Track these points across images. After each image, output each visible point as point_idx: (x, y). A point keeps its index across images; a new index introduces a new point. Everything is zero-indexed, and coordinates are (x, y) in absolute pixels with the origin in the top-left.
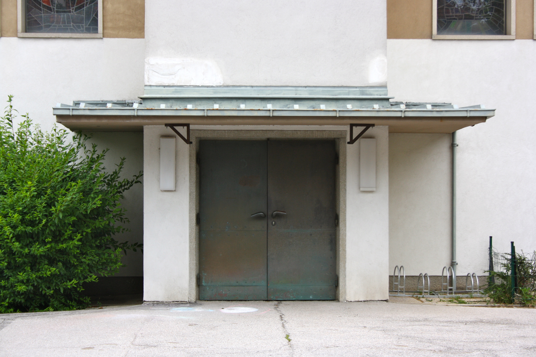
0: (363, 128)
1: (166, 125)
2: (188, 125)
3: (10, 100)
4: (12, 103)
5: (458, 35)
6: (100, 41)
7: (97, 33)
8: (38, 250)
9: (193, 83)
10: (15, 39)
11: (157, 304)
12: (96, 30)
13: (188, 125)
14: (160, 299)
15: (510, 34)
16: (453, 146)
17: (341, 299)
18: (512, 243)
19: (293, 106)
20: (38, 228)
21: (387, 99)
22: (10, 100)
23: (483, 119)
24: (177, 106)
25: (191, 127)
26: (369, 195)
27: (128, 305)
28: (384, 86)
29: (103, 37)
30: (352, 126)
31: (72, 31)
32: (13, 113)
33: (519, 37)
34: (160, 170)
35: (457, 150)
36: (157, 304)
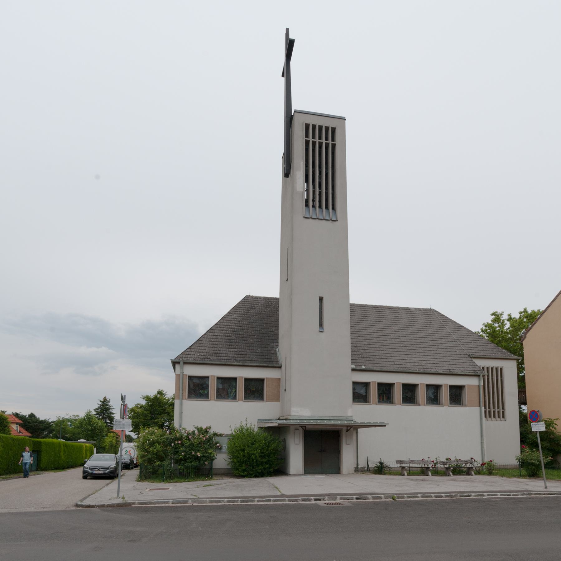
0: (350, 428)
1: (300, 426)
2: (305, 426)
3: (246, 419)
4: (247, 420)
5: (274, 402)
6: (265, 403)
7: (208, 399)
8: (265, 460)
9: (303, 415)
10: (242, 402)
11: (294, 475)
12: (236, 399)
13: (305, 426)
14: (295, 474)
15: (371, 403)
16: (357, 432)
17: (342, 473)
18: (381, 458)
19: (546, 428)
20: (135, 449)
21: (353, 420)
22: (246, 419)
23: (385, 426)
24: (301, 421)
25: (306, 427)
26: (349, 446)
27: (280, 475)
28: (352, 417)
29: (239, 401)
30: (347, 427)
31: (255, 400)
32: (247, 423)
33: (373, 404)
34: (295, 438)
35: (358, 433)
36: (294, 475)
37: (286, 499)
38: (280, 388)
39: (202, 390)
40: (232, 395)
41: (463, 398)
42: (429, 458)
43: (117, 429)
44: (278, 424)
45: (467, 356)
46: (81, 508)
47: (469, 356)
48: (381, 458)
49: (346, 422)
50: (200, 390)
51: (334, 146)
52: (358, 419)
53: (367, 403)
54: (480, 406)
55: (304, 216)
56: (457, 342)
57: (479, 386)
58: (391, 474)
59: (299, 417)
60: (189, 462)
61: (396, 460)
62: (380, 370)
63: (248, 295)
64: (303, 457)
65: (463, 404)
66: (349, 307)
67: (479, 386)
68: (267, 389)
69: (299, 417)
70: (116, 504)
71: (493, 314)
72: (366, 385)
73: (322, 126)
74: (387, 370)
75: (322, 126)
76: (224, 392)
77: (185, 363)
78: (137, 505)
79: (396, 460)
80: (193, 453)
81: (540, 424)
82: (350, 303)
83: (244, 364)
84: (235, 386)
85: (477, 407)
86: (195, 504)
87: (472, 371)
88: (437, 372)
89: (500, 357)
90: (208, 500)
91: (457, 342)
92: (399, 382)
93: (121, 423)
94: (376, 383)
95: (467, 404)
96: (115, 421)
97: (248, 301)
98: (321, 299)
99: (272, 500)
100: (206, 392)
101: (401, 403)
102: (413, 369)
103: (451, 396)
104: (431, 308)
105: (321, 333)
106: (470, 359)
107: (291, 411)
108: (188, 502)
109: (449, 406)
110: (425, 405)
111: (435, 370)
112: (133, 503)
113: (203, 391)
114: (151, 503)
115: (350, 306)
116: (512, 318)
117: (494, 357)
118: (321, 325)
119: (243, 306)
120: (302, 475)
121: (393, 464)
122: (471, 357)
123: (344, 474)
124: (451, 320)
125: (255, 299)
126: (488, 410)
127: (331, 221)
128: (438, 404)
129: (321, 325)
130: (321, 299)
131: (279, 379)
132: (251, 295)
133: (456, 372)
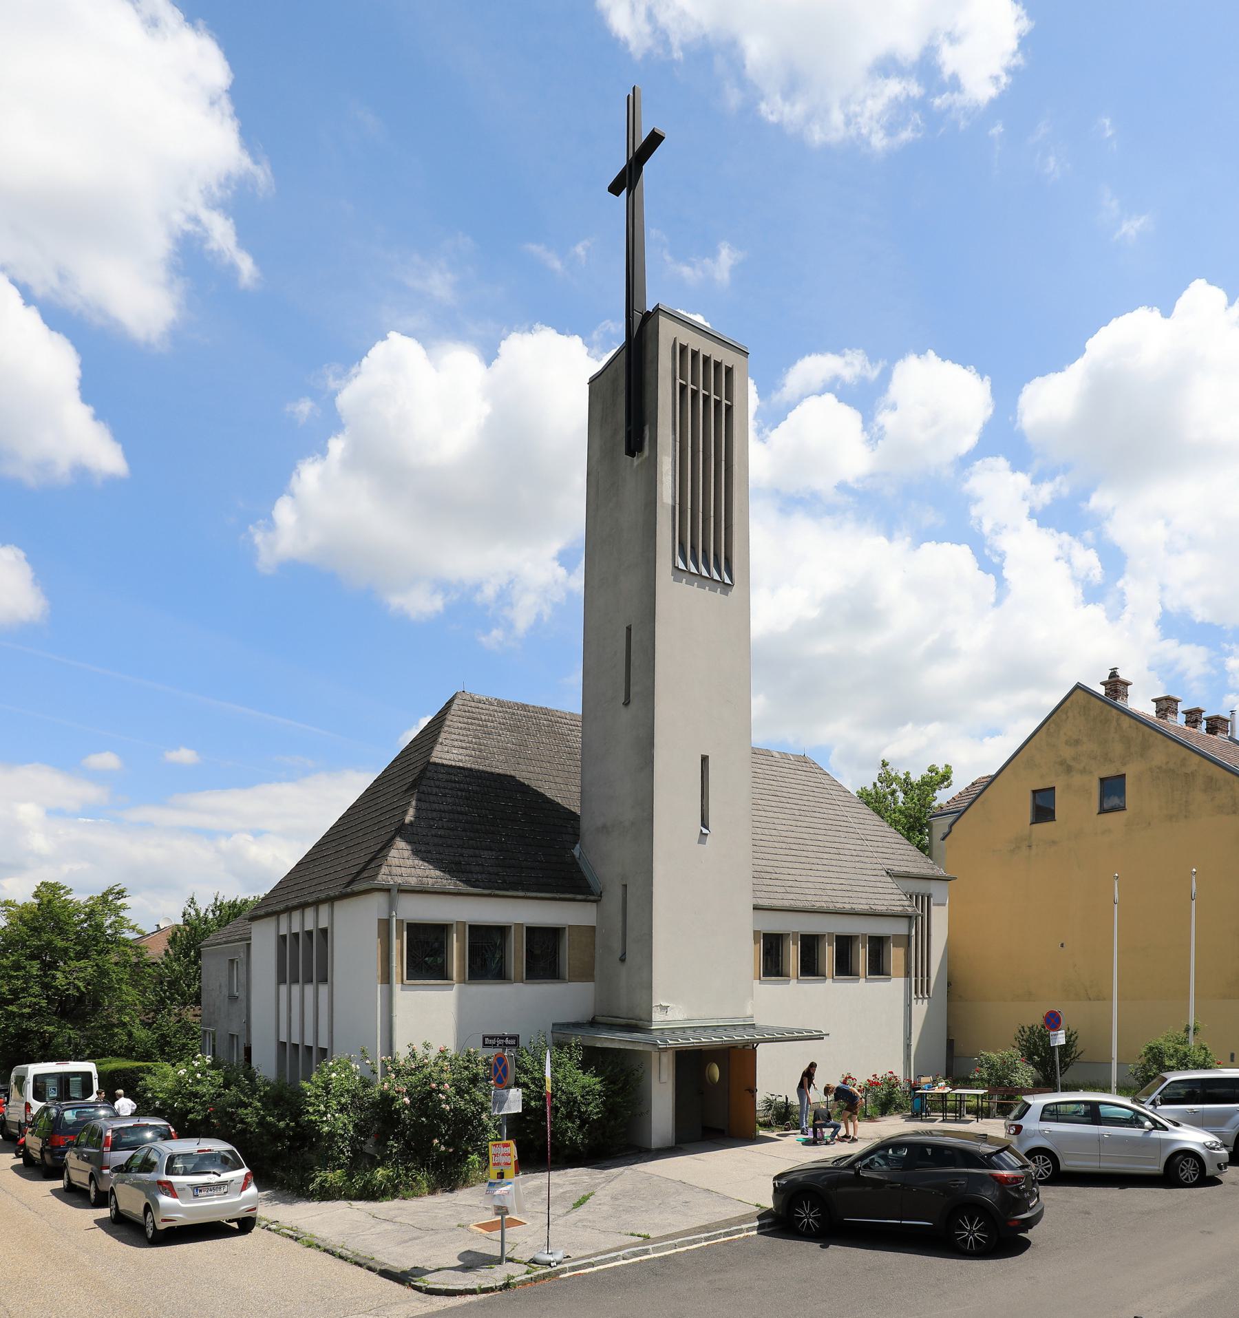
38: (594, 949)
39: (431, 956)
40: (494, 966)
45: (885, 874)
47: (888, 873)
50: (425, 957)
51: (729, 409)
56: (862, 839)
57: (909, 937)
68: (567, 954)
73: (686, 347)
75: (686, 347)
76: (478, 960)
81: (454, 760)
84: (500, 944)
91: (862, 839)
97: (466, 709)
98: (705, 759)
100: (439, 960)
113: (432, 958)
118: (704, 823)
119: (462, 725)
129: (704, 823)
130: (705, 759)
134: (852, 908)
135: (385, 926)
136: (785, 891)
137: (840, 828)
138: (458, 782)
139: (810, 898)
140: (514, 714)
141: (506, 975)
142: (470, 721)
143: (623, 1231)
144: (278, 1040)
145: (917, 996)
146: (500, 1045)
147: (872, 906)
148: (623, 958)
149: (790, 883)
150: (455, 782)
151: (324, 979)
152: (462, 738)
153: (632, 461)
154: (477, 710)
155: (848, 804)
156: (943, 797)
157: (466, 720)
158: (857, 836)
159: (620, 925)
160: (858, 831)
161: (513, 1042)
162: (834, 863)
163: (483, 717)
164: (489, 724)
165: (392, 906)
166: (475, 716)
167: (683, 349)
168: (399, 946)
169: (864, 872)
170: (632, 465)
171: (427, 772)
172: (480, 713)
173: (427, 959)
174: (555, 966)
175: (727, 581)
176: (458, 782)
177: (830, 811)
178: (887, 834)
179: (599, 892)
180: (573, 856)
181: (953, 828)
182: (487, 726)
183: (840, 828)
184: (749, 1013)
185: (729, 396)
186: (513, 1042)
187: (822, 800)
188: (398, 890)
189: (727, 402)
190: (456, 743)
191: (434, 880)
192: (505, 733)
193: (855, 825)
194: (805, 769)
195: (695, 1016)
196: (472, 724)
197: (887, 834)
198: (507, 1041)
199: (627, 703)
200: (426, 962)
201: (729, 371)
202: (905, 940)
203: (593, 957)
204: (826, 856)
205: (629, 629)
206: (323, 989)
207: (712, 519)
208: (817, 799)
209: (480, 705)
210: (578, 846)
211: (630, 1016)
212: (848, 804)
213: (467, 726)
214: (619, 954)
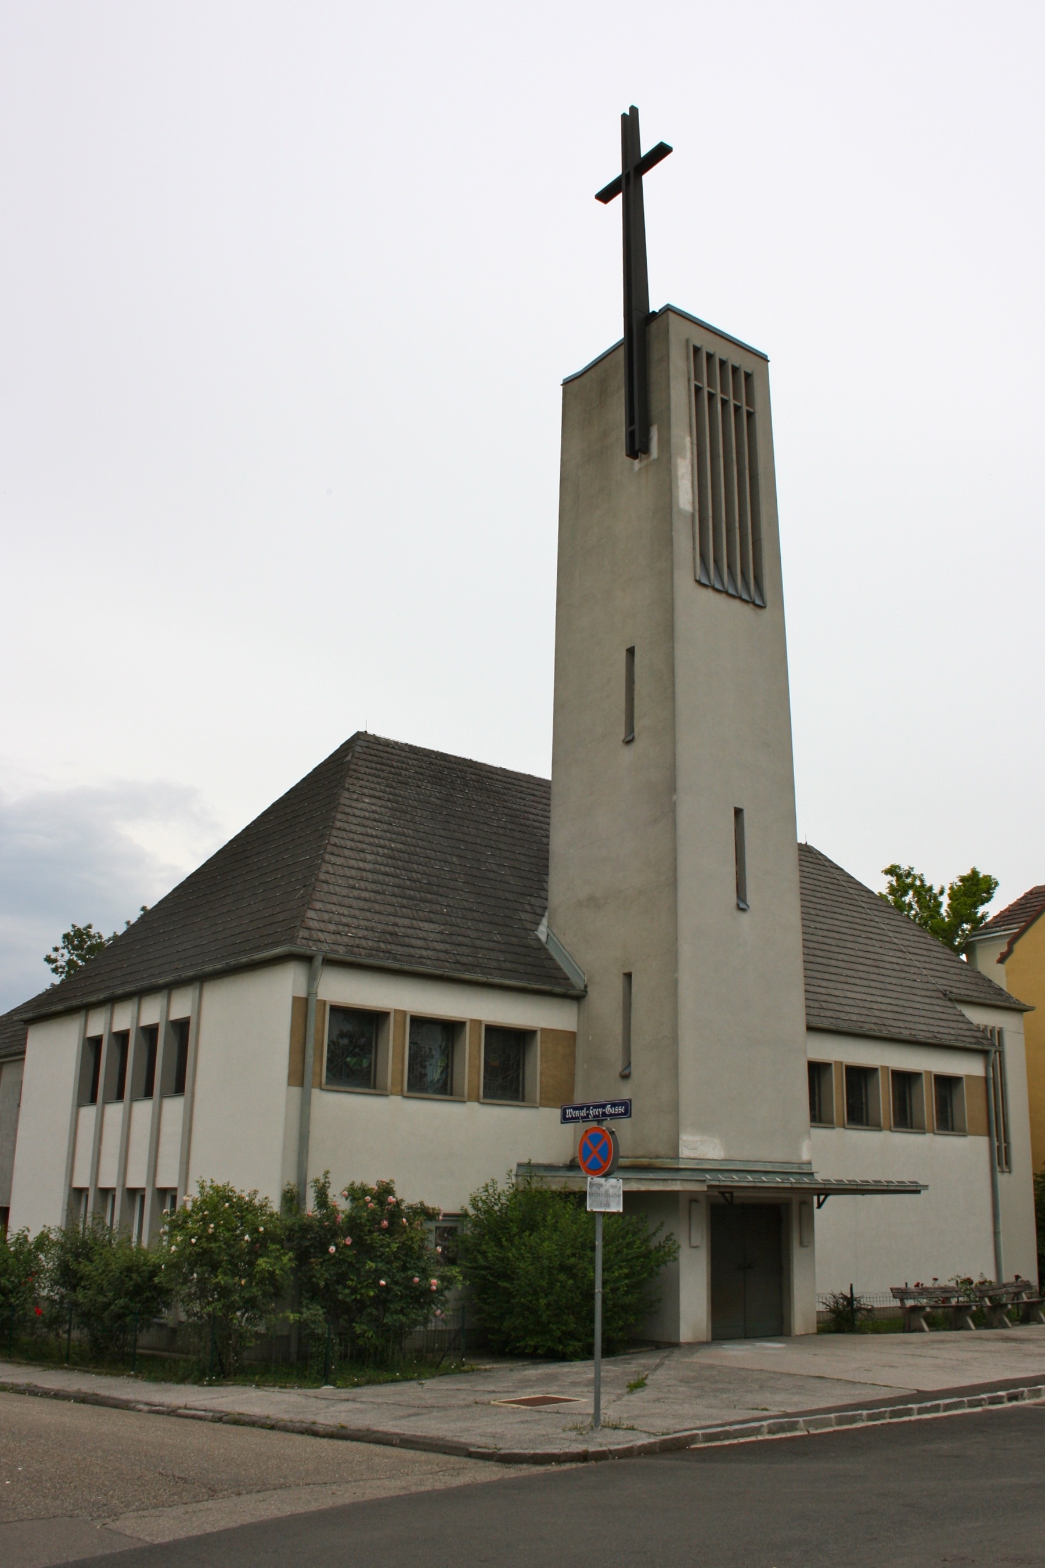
18: (851, 1285)
33: (838, 1126)
37: (963, 1401)
38: (574, 1063)
39: (354, 1055)
41: (955, 1112)
42: (936, 1279)
43: (595, 1210)
44: (709, 1187)
46: (567, 1466)
47: (945, 995)
48: (851, 1285)
49: (750, 1178)
50: (347, 1057)
51: (750, 415)
52: (825, 1173)
53: (516, 1099)
54: (989, 1134)
55: (698, 578)
58: (876, 1331)
59: (698, 1164)
60: (396, 1312)
61: (891, 1289)
62: (832, 1027)
63: (362, 730)
64: (708, 1283)
65: (955, 1128)
66: (797, 853)
67: (986, 1079)
69: (698, 1164)
70: (658, 1445)
71: (892, 871)
72: (451, 1028)
74: (820, 1025)
77: (331, 962)
78: (701, 1442)
79: (891, 1289)
80: (417, 1279)
82: (799, 841)
83: (491, 980)
85: (297, 1086)
86: (813, 1431)
87: (973, 1040)
88: (912, 1038)
89: (993, 1002)
90: (832, 1416)
92: (840, 1060)
93: (603, 1190)
94: (480, 1027)
95: (967, 1128)
96: (591, 1183)
98: (738, 812)
99: (942, 1406)
101: (844, 1121)
102: (867, 1026)
103: (332, 1047)
104: (809, 844)
105: (742, 915)
106: (949, 1004)
107: (681, 1142)
108: (798, 1427)
109: (893, 1129)
110: (934, 1130)
111: (908, 1033)
112: (693, 1438)
113: (355, 1060)
114: (727, 1435)
115: (799, 850)
116: (893, 880)
117: (989, 1002)
119: (373, 771)
120: (707, 1343)
121: (878, 1299)
122: (950, 1000)
123: (797, 1336)
124: (860, 884)
125: (393, 751)
126: (1003, 1145)
127: (751, 605)
128: (369, 1087)
130: (738, 812)
131: (572, 1035)
132: (370, 732)
133: (947, 1040)
134: (911, 1035)
135: (302, 1007)
136: (819, 1006)
137: (871, 936)
138: (377, 837)
139: (854, 1018)
140: (431, 763)
141: (454, 1086)
142: (379, 766)
143: (760, 1408)
144: (70, 1185)
145: (1002, 1168)
146: (595, 1116)
147: (937, 1035)
148: (626, 1072)
149: (824, 998)
150: (372, 836)
151: (179, 1086)
152: (372, 785)
153: (632, 464)
154: (386, 755)
155: (874, 907)
156: (991, 909)
157: (374, 765)
158: (895, 947)
159: (618, 1028)
160: (896, 941)
161: (621, 1110)
162: (873, 977)
163: (410, 762)
164: (403, 772)
165: (312, 980)
166: (384, 761)
167: (697, 350)
168: (322, 1031)
169: (915, 991)
170: (632, 468)
171: (336, 822)
172: (389, 759)
173: (348, 1059)
174: (518, 1085)
175: (758, 602)
176: (377, 837)
177: (855, 914)
178: (932, 948)
179: (582, 987)
180: (538, 940)
181: (1017, 947)
182: (400, 775)
183: (871, 936)
184: (805, 1156)
185: (750, 401)
186: (621, 1110)
187: (841, 899)
188: (323, 960)
189: (748, 409)
190: (366, 791)
191: (367, 951)
192: (424, 784)
193: (891, 934)
194: (810, 860)
195: (735, 1155)
196: (382, 771)
197: (932, 948)
198: (608, 1109)
199: (629, 742)
200: (347, 1064)
201: (748, 376)
202: (982, 1082)
203: (572, 1075)
204: (861, 968)
205: (631, 652)
206: (174, 1107)
207: (737, 531)
208: (834, 898)
209: (389, 749)
210: (545, 921)
211: (640, 1153)
212: (874, 907)
213: (376, 772)
214: (619, 1067)
